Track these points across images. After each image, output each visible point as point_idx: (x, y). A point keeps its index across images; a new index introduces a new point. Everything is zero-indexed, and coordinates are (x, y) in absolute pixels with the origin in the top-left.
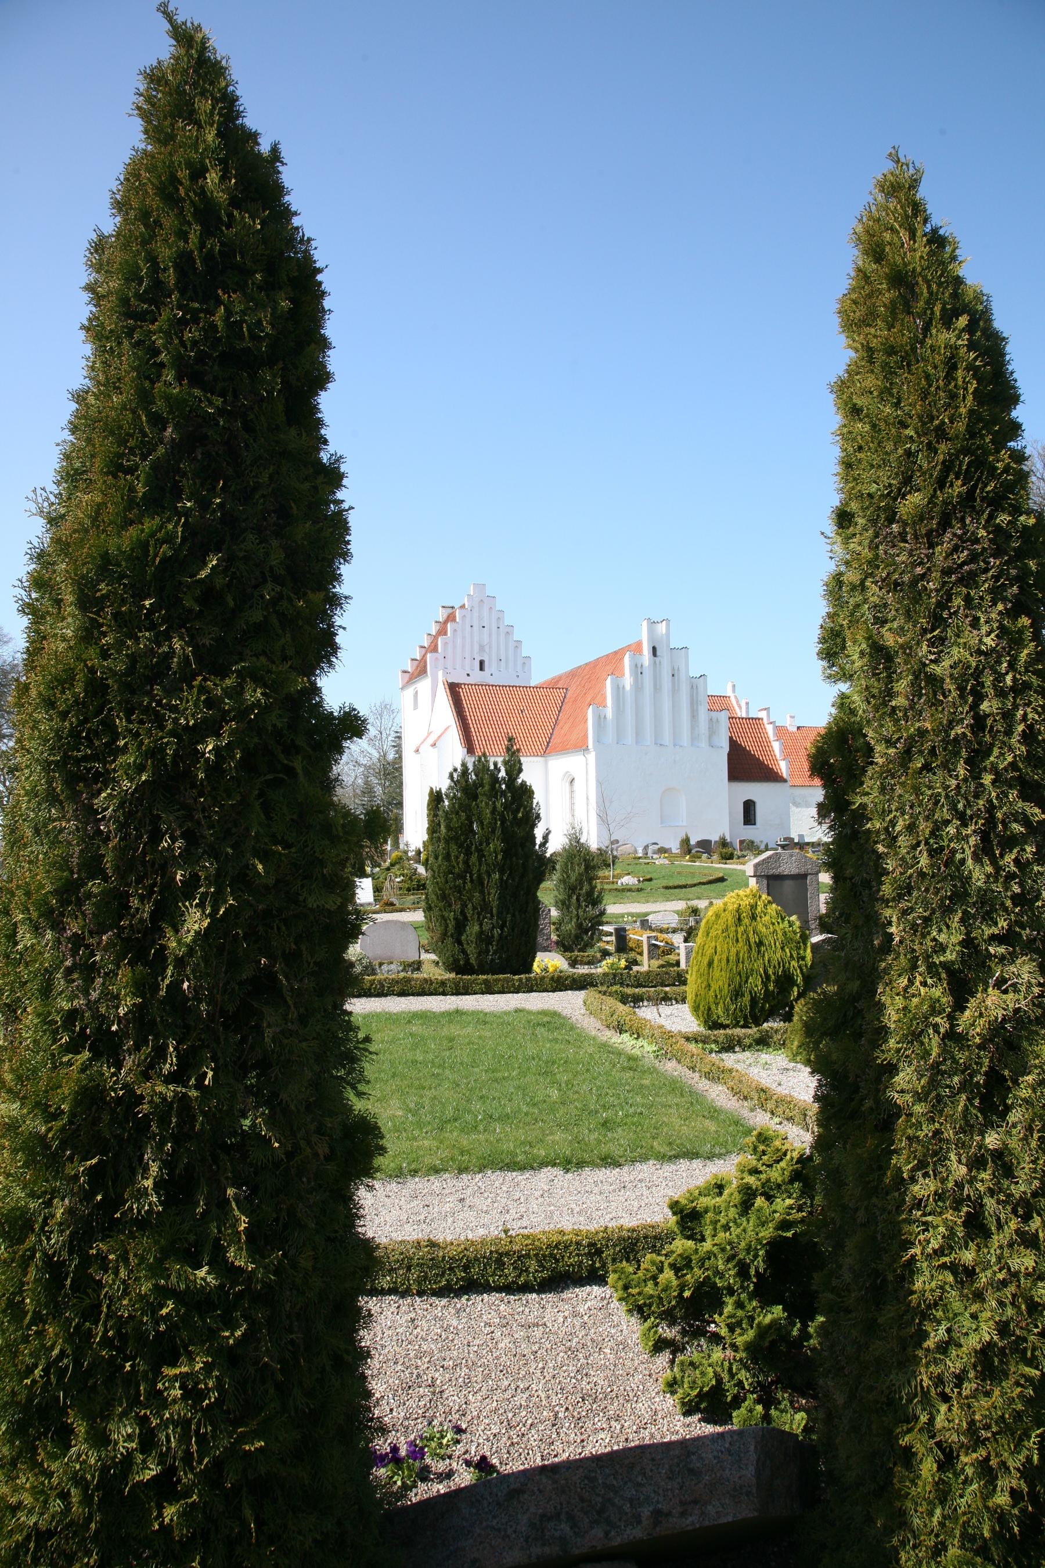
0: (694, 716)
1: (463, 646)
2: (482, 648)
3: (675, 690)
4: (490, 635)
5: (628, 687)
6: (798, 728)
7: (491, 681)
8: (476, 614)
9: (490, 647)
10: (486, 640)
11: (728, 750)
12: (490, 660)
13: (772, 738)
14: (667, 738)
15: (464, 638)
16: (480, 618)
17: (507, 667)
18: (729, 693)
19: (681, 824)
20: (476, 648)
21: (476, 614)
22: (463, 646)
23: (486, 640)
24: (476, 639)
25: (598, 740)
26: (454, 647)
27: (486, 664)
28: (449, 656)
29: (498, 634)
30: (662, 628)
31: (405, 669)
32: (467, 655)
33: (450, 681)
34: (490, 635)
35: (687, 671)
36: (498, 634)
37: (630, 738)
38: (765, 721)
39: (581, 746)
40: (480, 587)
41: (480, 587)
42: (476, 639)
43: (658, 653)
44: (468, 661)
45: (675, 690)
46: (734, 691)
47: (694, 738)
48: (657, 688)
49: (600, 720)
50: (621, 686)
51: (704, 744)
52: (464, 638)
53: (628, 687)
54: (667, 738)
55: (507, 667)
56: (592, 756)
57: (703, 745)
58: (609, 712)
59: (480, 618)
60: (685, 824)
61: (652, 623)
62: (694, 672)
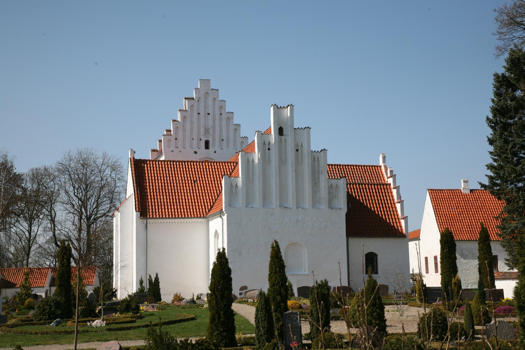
0: (315, 183)
1: (192, 130)
2: (207, 131)
3: (298, 162)
4: (214, 121)
5: (256, 161)
6: (471, 191)
7: (216, 158)
8: (202, 103)
9: (214, 130)
10: (210, 124)
11: (346, 210)
12: (214, 140)
13: (396, 201)
14: (291, 202)
15: (192, 123)
16: (206, 107)
17: (228, 146)
18: (381, 163)
19: (303, 273)
20: (202, 130)
21: (202, 103)
22: (192, 130)
23: (210, 124)
24: (202, 123)
25: (229, 204)
26: (184, 130)
27: (211, 143)
28: (180, 137)
29: (221, 119)
30: (287, 112)
31: (154, 148)
32: (195, 136)
33: (137, 157)
34: (214, 121)
35: (309, 146)
36: (221, 119)
37: (258, 202)
38: (392, 186)
39: (220, 213)
40: (205, 82)
41: (205, 82)
42: (202, 123)
43: (284, 133)
44: (195, 142)
45: (298, 162)
46: (384, 161)
47: (315, 202)
48: (282, 161)
49: (232, 189)
50: (251, 160)
51: (324, 206)
52: (192, 123)
53: (256, 161)
54: (291, 202)
55: (228, 146)
56: (225, 217)
57: (324, 207)
58: (240, 181)
59: (206, 107)
60: (307, 273)
61: (278, 108)
62: (315, 147)
